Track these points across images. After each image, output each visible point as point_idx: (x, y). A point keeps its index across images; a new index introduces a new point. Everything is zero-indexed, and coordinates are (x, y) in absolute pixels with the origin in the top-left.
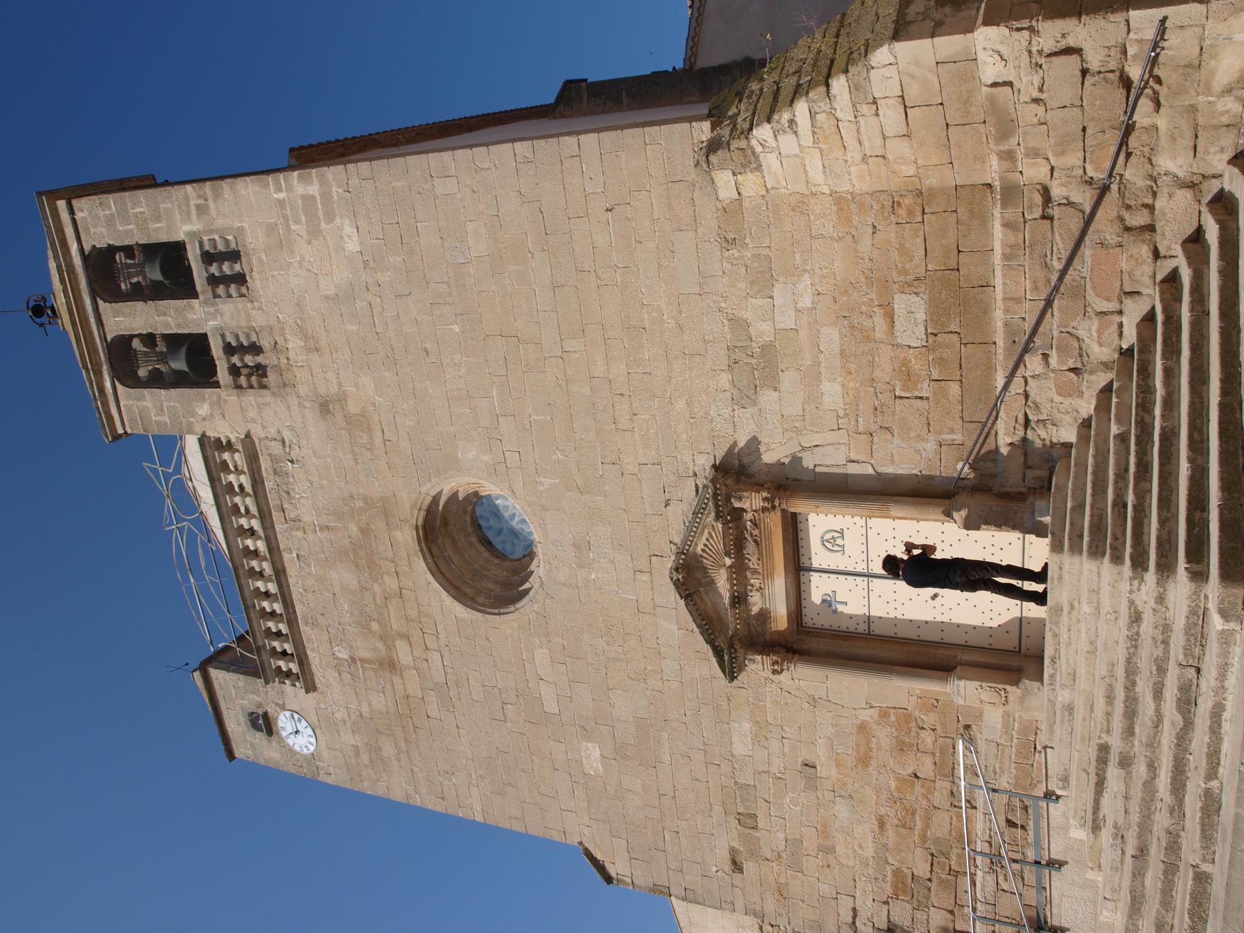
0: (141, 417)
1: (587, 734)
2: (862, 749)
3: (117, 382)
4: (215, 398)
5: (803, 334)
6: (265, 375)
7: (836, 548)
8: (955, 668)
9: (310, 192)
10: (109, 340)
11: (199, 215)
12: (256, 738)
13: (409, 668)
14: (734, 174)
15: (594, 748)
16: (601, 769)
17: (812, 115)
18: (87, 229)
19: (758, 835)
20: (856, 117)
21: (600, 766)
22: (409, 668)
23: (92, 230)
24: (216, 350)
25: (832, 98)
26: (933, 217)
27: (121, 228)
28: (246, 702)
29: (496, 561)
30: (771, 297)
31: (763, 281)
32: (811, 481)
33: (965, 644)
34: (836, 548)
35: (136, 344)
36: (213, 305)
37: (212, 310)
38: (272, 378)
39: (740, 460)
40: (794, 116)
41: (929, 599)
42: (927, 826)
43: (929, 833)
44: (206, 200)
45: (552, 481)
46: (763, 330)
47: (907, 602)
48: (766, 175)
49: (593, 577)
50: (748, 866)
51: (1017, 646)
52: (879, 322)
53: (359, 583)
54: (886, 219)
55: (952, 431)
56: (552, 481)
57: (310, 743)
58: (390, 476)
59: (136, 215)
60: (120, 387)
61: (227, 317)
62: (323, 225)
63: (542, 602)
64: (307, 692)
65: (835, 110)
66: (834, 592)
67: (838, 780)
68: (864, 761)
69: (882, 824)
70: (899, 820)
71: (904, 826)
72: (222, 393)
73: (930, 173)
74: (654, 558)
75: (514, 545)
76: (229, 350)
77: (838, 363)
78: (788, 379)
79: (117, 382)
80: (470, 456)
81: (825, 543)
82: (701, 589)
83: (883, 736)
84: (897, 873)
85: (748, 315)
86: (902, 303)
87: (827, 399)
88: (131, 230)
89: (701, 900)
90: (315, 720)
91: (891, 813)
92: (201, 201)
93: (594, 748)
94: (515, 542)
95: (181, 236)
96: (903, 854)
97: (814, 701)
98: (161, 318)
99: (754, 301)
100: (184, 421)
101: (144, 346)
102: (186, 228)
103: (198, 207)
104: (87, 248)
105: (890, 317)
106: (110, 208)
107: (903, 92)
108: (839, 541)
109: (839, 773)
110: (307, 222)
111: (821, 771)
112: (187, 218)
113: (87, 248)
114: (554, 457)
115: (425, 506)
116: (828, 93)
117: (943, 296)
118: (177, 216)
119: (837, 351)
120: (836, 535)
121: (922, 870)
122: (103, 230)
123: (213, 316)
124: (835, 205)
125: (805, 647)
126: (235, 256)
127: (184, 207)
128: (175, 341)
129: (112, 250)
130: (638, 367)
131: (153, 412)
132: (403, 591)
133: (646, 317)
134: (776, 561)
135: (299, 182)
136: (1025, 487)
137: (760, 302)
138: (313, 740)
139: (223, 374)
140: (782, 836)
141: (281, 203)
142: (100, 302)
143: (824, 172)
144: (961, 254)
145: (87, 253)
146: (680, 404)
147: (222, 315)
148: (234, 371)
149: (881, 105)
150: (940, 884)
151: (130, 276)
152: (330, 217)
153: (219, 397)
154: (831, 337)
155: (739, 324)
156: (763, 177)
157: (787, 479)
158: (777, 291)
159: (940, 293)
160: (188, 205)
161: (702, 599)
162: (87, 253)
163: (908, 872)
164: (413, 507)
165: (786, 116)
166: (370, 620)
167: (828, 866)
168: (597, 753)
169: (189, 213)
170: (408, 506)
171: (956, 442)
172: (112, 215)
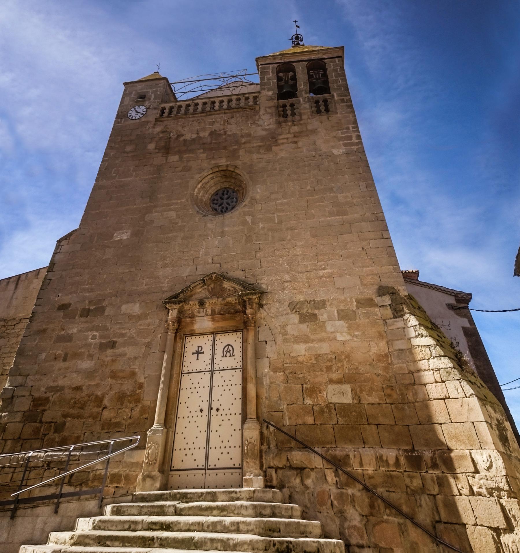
0: (266, 72)
1: (135, 234)
2: (121, 374)
3: (278, 64)
4: (273, 98)
5: (323, 335)
6: (283, 117)
7: (225, 353)
8: (166, 428)
9: (353, 139)
10: (294, 64)
11: (340, 99)
12: (134, 95)
13: (166, 160)
14: (390, 305)
15: (127, 236)
16: (117, 239)
17: (429, 346)
18: (331, 62)
19: (77, 318)
20: (432, 370)
21: (118, 239)
22: (166, 160)
23: (332, 64)
24: (291, 100)
25: (439, 358)
26: (390, 409)
27: (333, 74)
28: (150, 94)
29: (210, 197)
30: (338, 320)
31: (343, 315)
32: (259, 339)
33: (174, 449)
34: (225, 353)
35: (291, 74)
36: (308, 101)
37: (306, 100)
38: (282, 119)
39: (265, 304)
40: (425, 337)
41: (200, 408)
42: (73, 417)
43: (69, 419)
44: (346, 102)
46: (323, 316)
47: (199, 394)
48: (392, 320)
49: (209, 238)
50: (61, 314)
51: (174, 468)
52: (335, 376)
53: (498, 451)
54: (384, 381)
55: (290, 418)
57: (132, 117)
59: (338, 80)
60: (276, 65)
61: (305, 106)
62: (341, 142)
64: (156, 119)
65: (434, 359)
66: (203, 353)
67: (104, 362)
68: (114, 375)
69: (78, 388)
70: (78, 400)
71: (75, 403)
72: (276, 101)
73: (412, 409)
74: (219, 265)
75: (216, 204)
76: (292, 105)
77: (314, 353)
78: (305, 327)
79: (278, 64)
80: (259, 190)
81: (227, 347)
82: (206, 287)
83: (128, 386)
84: (47, 400)
85: (328, 308)
86: (347, 388)
87: (296, 346)
88: (333, 77)
89: (44, 288)
90: (143, 120)
91: (83, 395)
92: (345, 101)
93: (127, 236)
95: (332, 93)
96: (58, 403)
97: (148, 345)
98: (302, 84)
99: (336, 311)
100: (265, 87)
101: (291, 77)
102: (335, 95)
103: (344, 99)
104: (326, 61)
105: (339, 382)
106: (340, 71)
107: (453, 399)
108: (228, 354)
109: (108, 362)
110: (342, 137)
111: (109, 352)
112: (338, 95)
113: (326, 61)
116: (441, 356)
117: (354, 414)
118: (340, 92)
119: (319, 352)
120: (231, 353)
121: (47, 417)
122: (332, 68)
123: (304, 101)
124: (385, 354)
125: (178, 339)
126: (327, 110)
127: (342, 94)
128: (295, 86)
129: (325, 70)
130: (301, 259)
131: (268, 76)
133: (323, 263)
134: (220, 323)
135: (357, 135)
136: (266, 468)
137: (336, 314)
138: (134, 118)
139: (282, 102)
140: (75, 330)
141: (348, 128)
142: (307, 63)
143: (400, 350)
144: (376, 426)
145: (324, 60)
146: (287, 277)
147: (304, 104)
148: (284, 106)
149: (442, 385)
150: (37, 428)
151: (315, 74)
152: (345, 145)
153: (273, 99)
154: (325, 348)
155: (322, 304)
156: (391, 319)
157: (259, 327)
158: (342, 323)
159: (355, 411)
160: (344, 96)
161: (201, 287)
162: (324, 60)
163: (46, 408)
165: (425, 333)
167: (55, 358)
168: (125, 237)
169: (341, 96)
171: (284, 422)
172: (338, 72)
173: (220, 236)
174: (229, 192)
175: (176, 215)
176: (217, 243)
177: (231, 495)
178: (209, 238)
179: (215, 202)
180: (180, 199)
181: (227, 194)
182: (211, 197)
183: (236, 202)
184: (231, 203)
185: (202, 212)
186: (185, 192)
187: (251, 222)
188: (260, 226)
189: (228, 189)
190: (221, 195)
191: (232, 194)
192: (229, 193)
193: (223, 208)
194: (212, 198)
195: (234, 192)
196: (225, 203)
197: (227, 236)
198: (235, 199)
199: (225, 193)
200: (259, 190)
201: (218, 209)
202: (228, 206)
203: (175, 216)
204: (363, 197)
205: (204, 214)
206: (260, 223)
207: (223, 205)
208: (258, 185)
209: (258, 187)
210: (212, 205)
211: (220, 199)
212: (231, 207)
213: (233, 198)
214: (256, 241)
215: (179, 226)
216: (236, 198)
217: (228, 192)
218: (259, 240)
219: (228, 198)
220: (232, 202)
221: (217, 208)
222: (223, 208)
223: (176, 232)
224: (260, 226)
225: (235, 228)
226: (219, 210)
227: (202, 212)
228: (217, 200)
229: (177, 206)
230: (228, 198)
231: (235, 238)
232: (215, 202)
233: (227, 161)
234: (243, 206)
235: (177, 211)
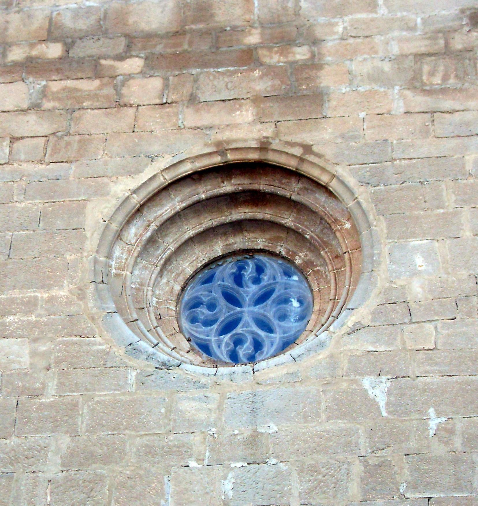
45: (382, 404)
56: (382, 404)
58: (362, 115)
63: (131, 363)
75: (208, 323)
80: (419, 260)
94: (215, 326)
114: (431, 411)
115: (272, 158)
132: (131, 111)
164: (307, 149)
166: (65, 44)
170: (306, 138)
173: (244, 459)
174: (268, 271)
175: (34, 354)
176: (228, 486)
177: (409, 418)
178: (193, 464)
179: (203, 312)
180: (45, 286)
181: (256, 281)
182: (183, 289)
183: (302, 317)
184: (275, 323)
185: (151, 350)
186: (69, 257)
187: (387, 404)
188: (433, 424)
189: (263, 258)
190: (229, 283)
191: (281, 279)
192: (265, 279)
193: (238, 341)
194: (186, 297)
195: (287, 274)
196: (247, 318)
197: (274, 461)
198: (295, 304)
199: (249, 271)
200: (419, 260)
201: (214, 346)
202: (262, 334)
203: (26, 360)
204: (69, 92)
205: (164, 357)
206: (431, 411)
207: (239, 330)
208: (414, 235)
209: (416, 249)
210: (186, 325)
211: (222, 302)
212: (277, 337)
213: (286, 301)
214: (414, 486)
215: (51, 406)
216: (300, 301)
217: (260, 270)
218: (430, 485)
219: (262, 299)
220: (283, 317)
221: (213, 339)
222: (238, 341)
223: (37, 431)
224: (433, 424)
225: (314, 427)
226: (222, 353)
227: (151, 350)
228: (211, 306)
229: (33, 318)
230: (262, 299)
231: (314, 470)
232: (203, 312)
233: (260, 120)
234: (345, 329)
235: (35, 340)
